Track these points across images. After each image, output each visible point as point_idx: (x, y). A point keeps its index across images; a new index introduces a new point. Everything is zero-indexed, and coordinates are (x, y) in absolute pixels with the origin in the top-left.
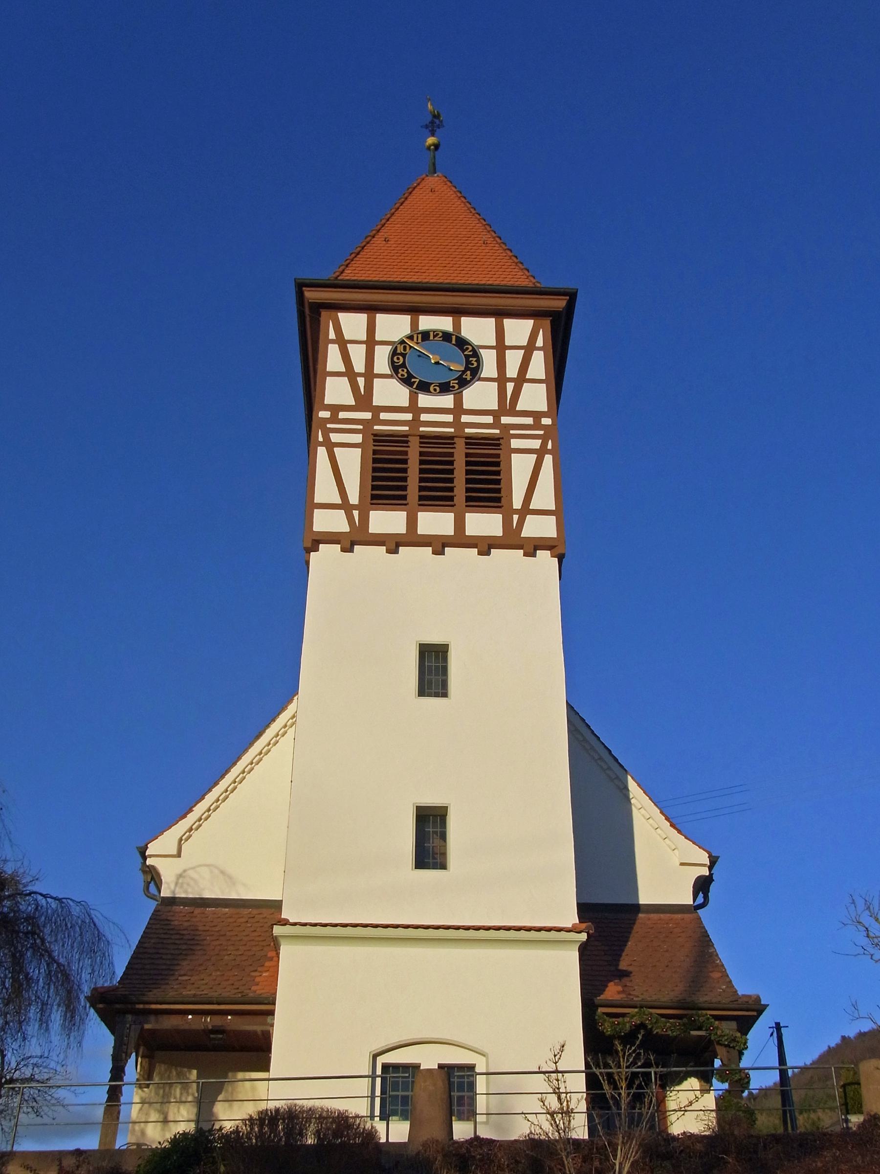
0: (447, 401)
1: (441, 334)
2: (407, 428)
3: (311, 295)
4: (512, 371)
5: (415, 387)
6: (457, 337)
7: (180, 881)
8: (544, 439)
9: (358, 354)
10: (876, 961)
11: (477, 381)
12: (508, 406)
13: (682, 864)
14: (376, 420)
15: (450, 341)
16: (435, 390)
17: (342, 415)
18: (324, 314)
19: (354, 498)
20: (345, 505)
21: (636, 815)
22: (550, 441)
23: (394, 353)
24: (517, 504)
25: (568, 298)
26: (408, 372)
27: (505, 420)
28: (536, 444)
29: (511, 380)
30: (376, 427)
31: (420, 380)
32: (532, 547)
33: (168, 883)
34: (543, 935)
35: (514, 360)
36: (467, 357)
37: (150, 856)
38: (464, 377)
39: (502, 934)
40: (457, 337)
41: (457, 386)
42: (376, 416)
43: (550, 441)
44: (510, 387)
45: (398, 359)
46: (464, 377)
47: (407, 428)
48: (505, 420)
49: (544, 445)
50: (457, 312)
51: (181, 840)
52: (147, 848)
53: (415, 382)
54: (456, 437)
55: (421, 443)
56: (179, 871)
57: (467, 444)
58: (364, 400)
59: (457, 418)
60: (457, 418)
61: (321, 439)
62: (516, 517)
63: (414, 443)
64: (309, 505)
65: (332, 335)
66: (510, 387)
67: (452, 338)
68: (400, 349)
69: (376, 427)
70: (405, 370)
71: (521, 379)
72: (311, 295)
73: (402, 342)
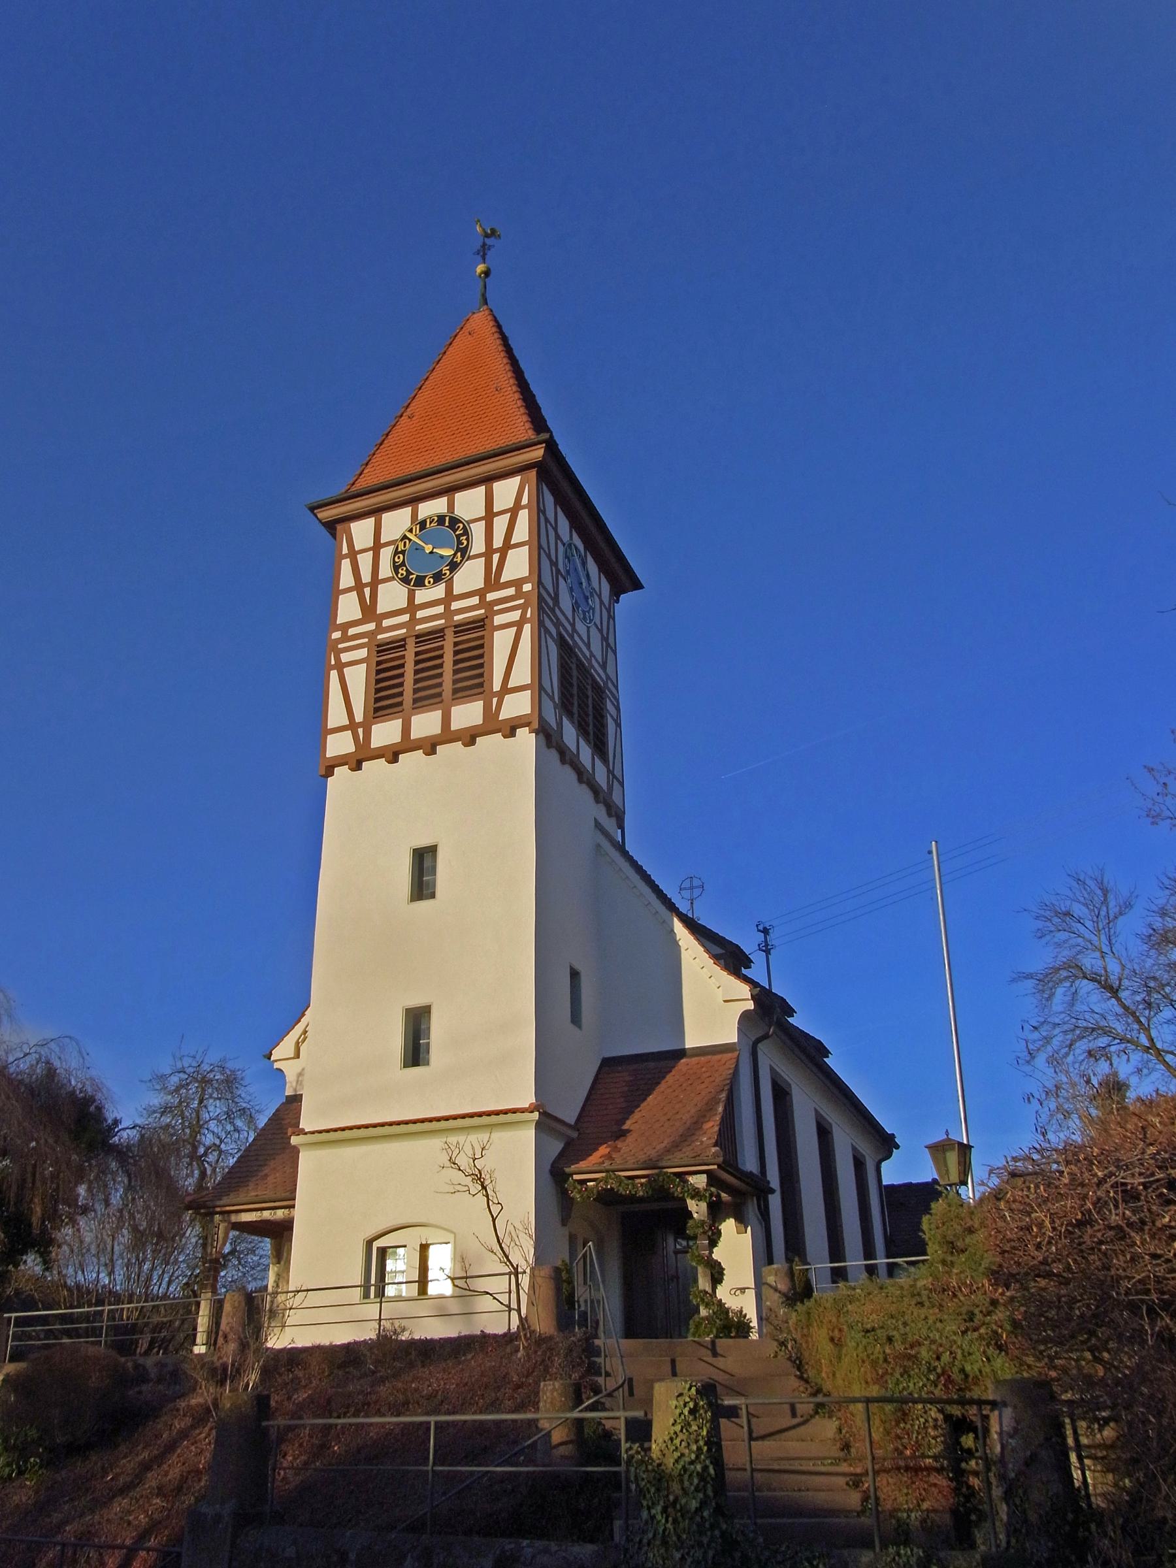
0: (439, 591)
1: (436, 519)
2: (404, 631)
3: (326, 514)
4: (366, 577)
5: (412, 584)
6: (451, 518)
7: (300, 1079)
8: (524, 607)
9: (365, 561)
10: (474, 1195)
11: (467, 560)
12: (493, 580)
13: (725, 1001)
14: (380, 629)
15: (443, 524)
16: (429, 582)
17: (352, 631)
18: (339, 527)
19: (359, 717)
20: (352, 726)
21: (686, 957)
22: (530, 609)
23: (396, 553)
24: (497, 687)
25: (544, 445)
26: (407, 570)
27: (491, 597)
28: (515, 616)
29: (366, 585)
30: (379, 637)
31: (417, 576)
32: (510, 729)
33: (291, 1082)
34: (451, 1123)
35: (500, 524)
36: (458, 537)
37: (276, 1061)
38: (455, 560)
39: (419, 1127)
40: (451, 518)
41: (448, 572)
42: (379, 625)
43: (530, 609)
44: (367, 591)
45: (399, 558)
46: (455, 560)
47: (404, 631)
48: (491, 597)
49: (523, 615)
50: (449, 490)
51: (297, 1043)
52: (271, 1054)
53: (412, 579)
54: (446, 628)
55: (416, 643)
56: (299, 1070)
57: (456, 632)
58: (369, 611)
59: (447, 607)
60: (447, 607)
61: (333, 662)
62: (495, 700)
63: (411, 643)
64: (323, 732)
65: (345, 550)
66: (367, 591)
67: (449, 523)
68: (401, 548)
69: (379, 637)
70: (405, 568)
71: (375, 582)
72: (326, 514)
73: (405, 537)
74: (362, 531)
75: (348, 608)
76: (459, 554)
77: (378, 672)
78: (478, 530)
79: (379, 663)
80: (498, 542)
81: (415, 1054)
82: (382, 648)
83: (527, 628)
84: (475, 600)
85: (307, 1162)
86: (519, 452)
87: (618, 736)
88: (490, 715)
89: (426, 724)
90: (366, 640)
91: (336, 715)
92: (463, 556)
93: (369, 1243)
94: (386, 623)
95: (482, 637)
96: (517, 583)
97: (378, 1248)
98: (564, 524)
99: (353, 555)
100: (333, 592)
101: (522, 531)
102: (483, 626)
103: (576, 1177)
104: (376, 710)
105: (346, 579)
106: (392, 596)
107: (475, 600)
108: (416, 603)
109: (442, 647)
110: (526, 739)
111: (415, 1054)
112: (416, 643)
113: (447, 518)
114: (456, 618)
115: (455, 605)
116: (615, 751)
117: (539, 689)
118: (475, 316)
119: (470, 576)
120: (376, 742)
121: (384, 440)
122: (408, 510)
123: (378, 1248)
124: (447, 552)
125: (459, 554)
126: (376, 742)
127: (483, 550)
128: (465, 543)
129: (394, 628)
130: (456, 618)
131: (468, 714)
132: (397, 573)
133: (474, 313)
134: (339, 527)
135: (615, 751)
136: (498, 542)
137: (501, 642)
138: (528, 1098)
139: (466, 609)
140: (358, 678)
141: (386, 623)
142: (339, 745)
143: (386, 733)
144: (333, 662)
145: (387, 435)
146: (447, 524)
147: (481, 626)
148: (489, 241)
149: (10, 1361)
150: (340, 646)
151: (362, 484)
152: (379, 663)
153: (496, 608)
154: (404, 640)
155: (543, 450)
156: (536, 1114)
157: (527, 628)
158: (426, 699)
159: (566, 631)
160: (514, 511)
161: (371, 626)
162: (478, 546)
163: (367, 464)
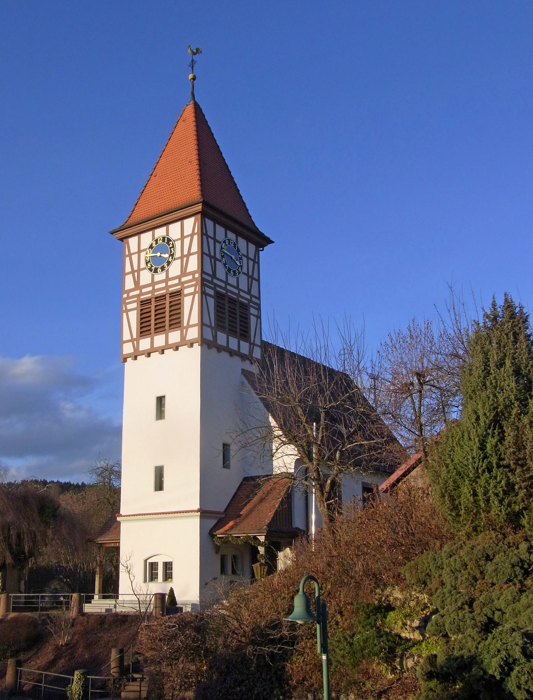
1: (162, 238)
4: (136, 268)
5: (153, 272)
12: (184, 272)
14: (141, 294)
17: (131, 294)
19: (135, 336)
20: (132, 340)
24: (185, 325)
25: (201, 204)
27: (183, 279)
41: (167, 266)
48: (183, 279)
55: (155, 301)
60: (166, 284)
61: (124, 309)
62: (185, 330)
65: (127, 253)
66: (136, 274)
74: (133, 242)
75: (129, 283)
76: (171, 257)
77: (141, 314)
78: (178, 244)
79: (141, 310)
80: (186, 252)
81: (159, 486)
82: (144, 303)
83: (197, 295)
84: (177, 281)
85: (124, 527)
86: (191, 207)
87: (259, 324)
88: (183, 337)
89: (159, 340)
90: (136, 299)
91: (126, 336)
92: (172, 258)
93: (146, 561)
94: (144, 290)
95: (180, 299)
96: (193, 273)
97: (149, 563)
98: (220, 231)
99: (130, 255)
100: (123, 274)
101: (195, 248)
102: (180, 294)
103: (218, 536)
104: (141, 333)
105: (128, 269)
106: (146, 277)
107: (177, 281)
108: (155, 281)
109: (165, 304)
110: (197, 348)
111: (159, 486)
112: (155, 301)
113: (166, 238)
114: (170, 289)
115: (170, 283)
116: (255, 331)
117: (202, 325)
118: (188, 107)
119: (175, 269)
120: (141, 348)
121: (144, 190)
122: (150, 233)
123: (149, 563)
124: (166, 256)
125: (171, 257)
126: (141, 348)
127: (180, 255)
128: (173, 251)
129: (147, 293)
130: (170, 289)
131: (174, 336)
132: (147, 266)
133: (187, 105)
134: (125, 240)
135: (255, 331)
136: (186, 252)
137: (187, 301)
138: (197, 506)
139: (174, 285)
140: (134, 316)
141: (144, 290)
142: (128, 349)
143: (145, 344)
144: (124, 309)
145: (145, 187)
146: (166, 242)
147: (179, 293)
148: (196, 58)
149: (12, 611)
150: (127, 301)
151: (131, 221)
152: (141, 310)
153: (185, 285)
154: (150, 299)
155: (201, 206)
156: (199, 513)
157: (197, 295)
158: (160, 329)
159: (220, 287)
160: (192, 236)
161: (137, 292)
162: (178, 254)
163: (136, 205)
